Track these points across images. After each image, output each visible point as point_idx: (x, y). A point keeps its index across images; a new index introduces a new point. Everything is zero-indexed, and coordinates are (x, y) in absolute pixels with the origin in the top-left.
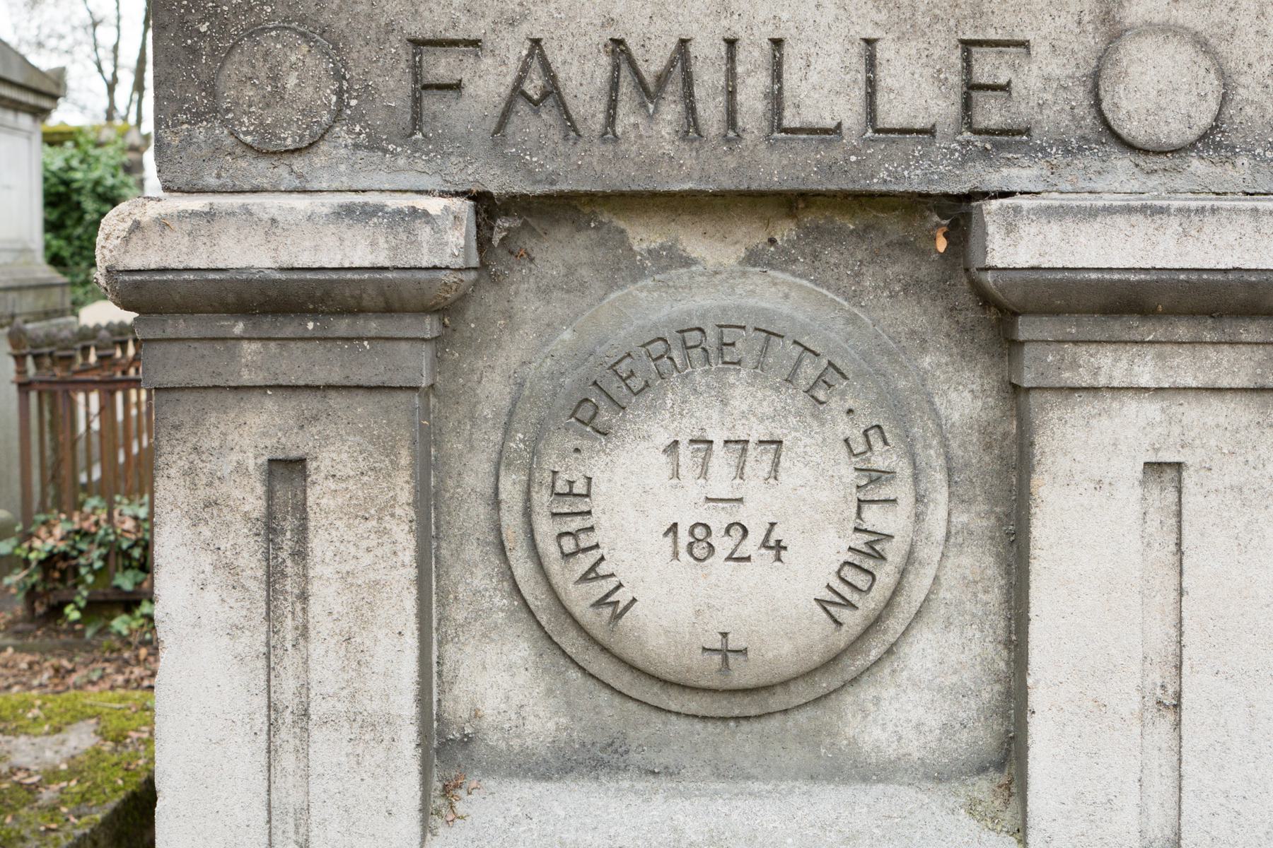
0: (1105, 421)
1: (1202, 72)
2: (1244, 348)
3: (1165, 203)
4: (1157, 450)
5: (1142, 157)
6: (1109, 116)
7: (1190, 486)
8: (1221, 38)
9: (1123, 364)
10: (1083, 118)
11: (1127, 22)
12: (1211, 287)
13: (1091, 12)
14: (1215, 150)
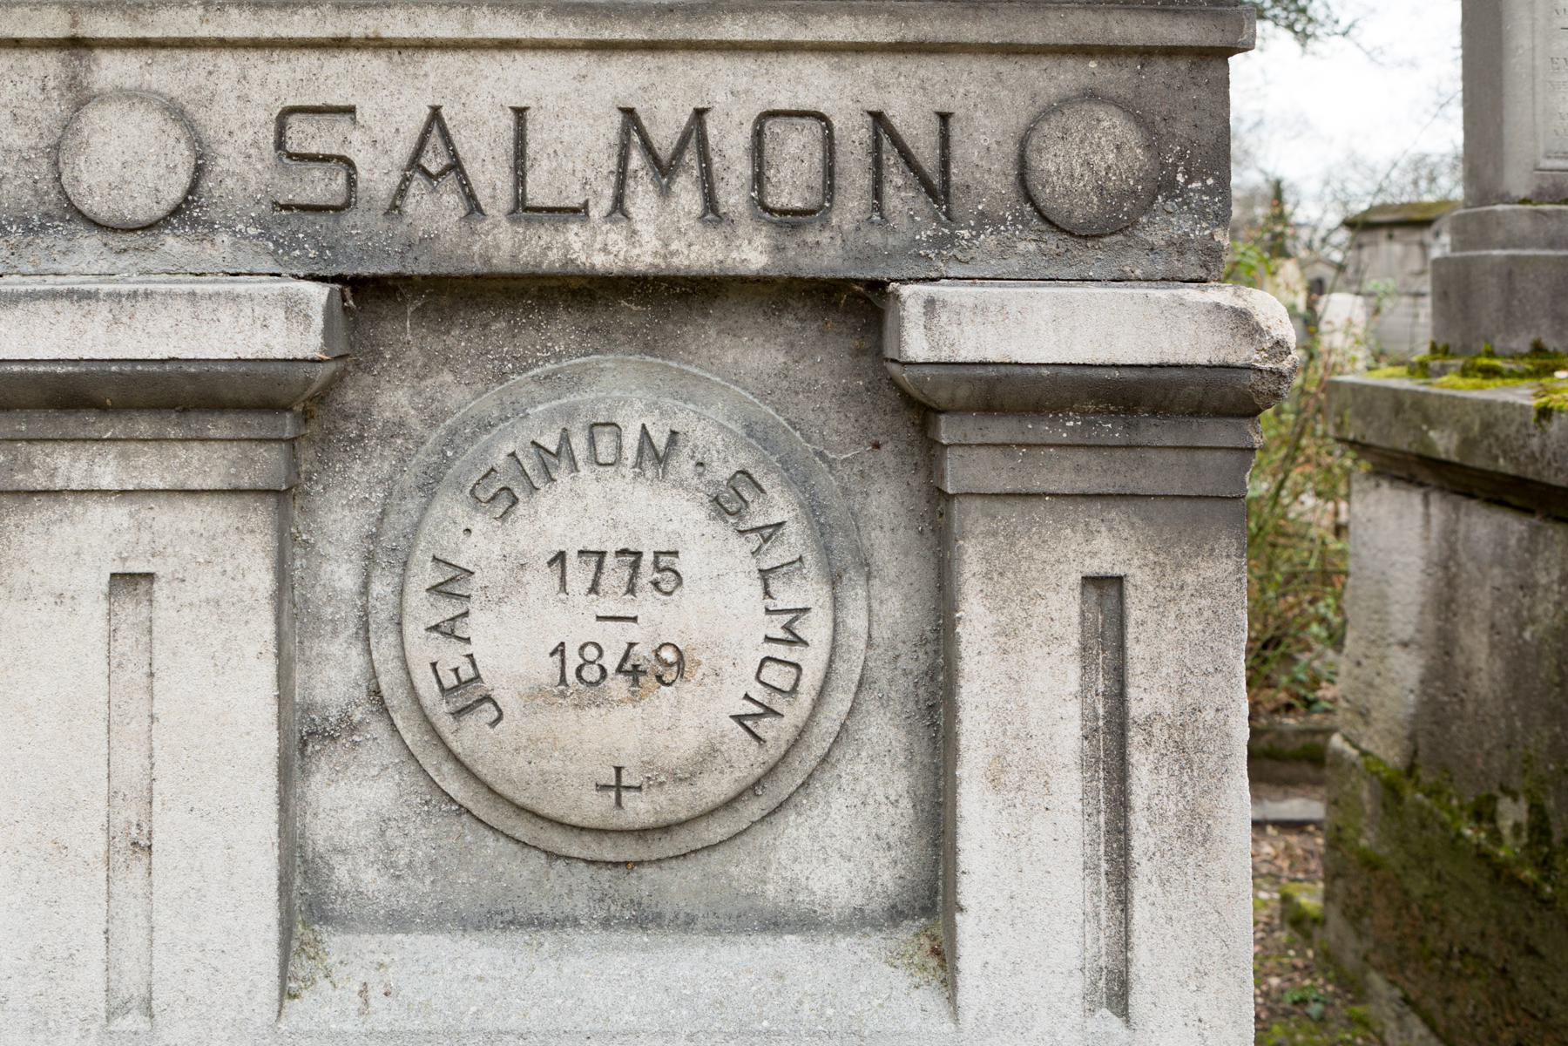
0: (67, 527)
1: (172, 142)
2: (216, 445)
3: (92, 287)
4: (124, 560)
5: (111, 235)
6: (69, 191)
7: (161, 599)
8: (200, 104)
9: (82, 464)
10: (47, 193)
11: (96, 88)
12: (152, 379)
13: (56, 78)
14: (192, 227)
